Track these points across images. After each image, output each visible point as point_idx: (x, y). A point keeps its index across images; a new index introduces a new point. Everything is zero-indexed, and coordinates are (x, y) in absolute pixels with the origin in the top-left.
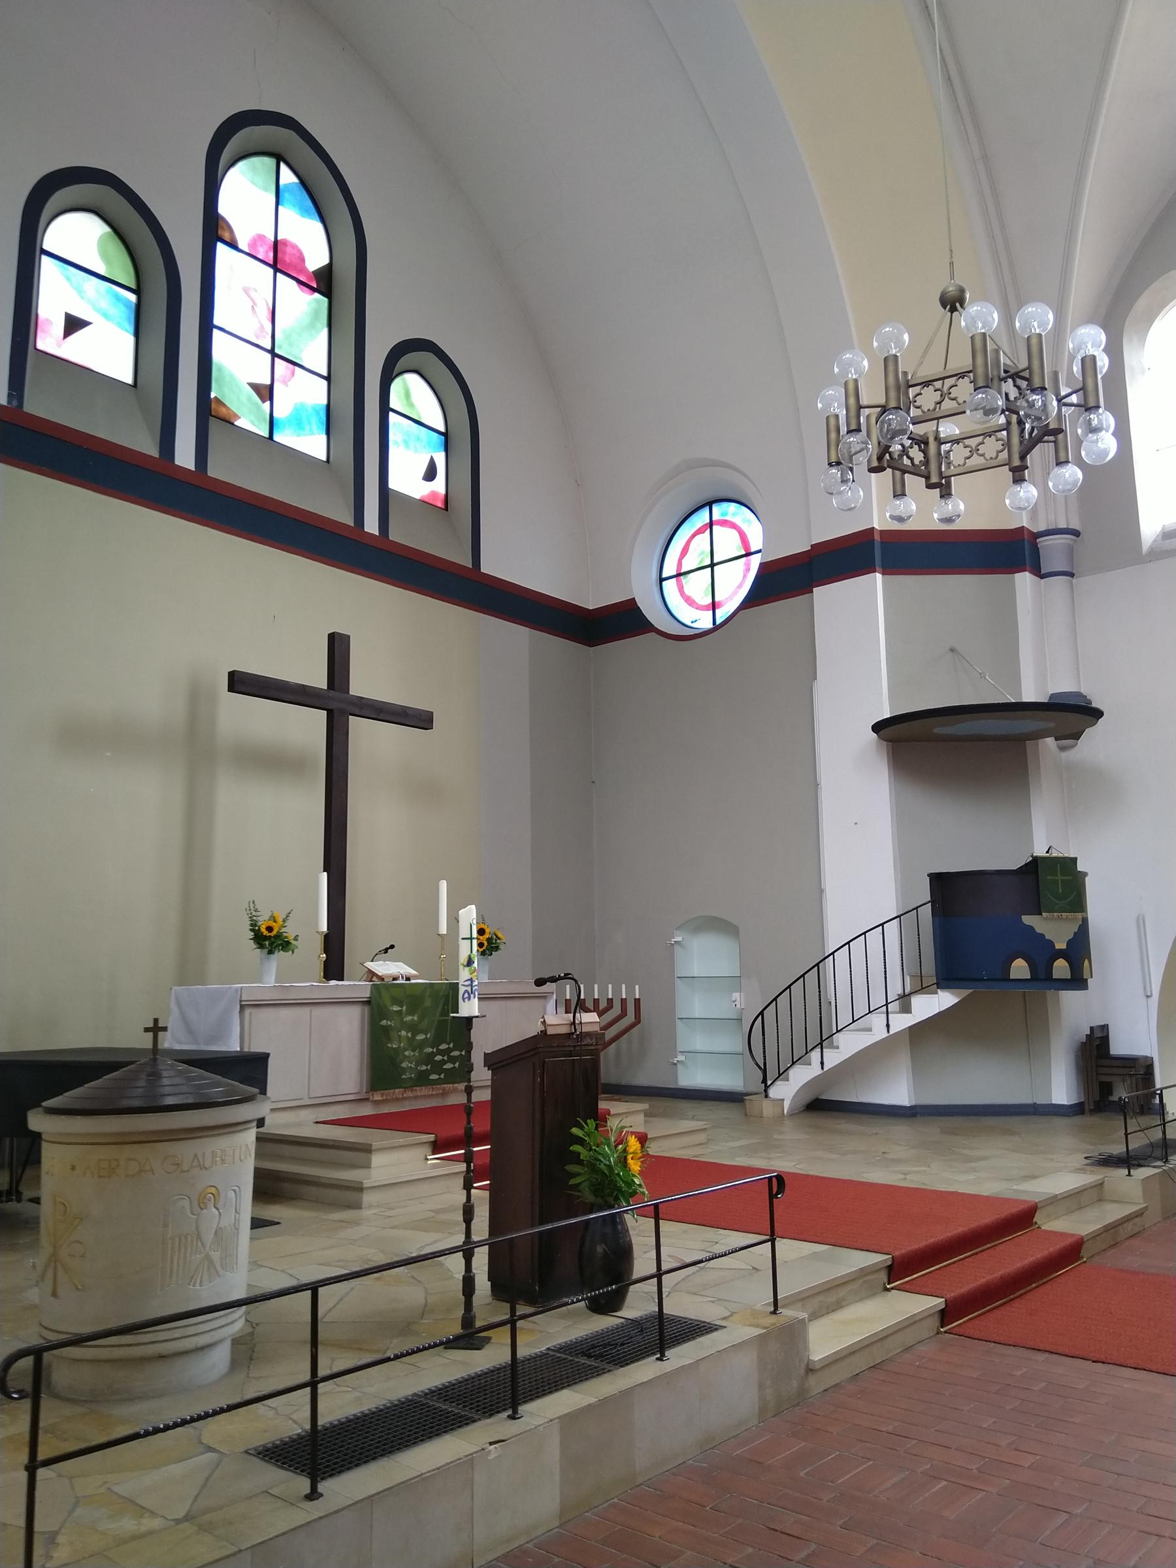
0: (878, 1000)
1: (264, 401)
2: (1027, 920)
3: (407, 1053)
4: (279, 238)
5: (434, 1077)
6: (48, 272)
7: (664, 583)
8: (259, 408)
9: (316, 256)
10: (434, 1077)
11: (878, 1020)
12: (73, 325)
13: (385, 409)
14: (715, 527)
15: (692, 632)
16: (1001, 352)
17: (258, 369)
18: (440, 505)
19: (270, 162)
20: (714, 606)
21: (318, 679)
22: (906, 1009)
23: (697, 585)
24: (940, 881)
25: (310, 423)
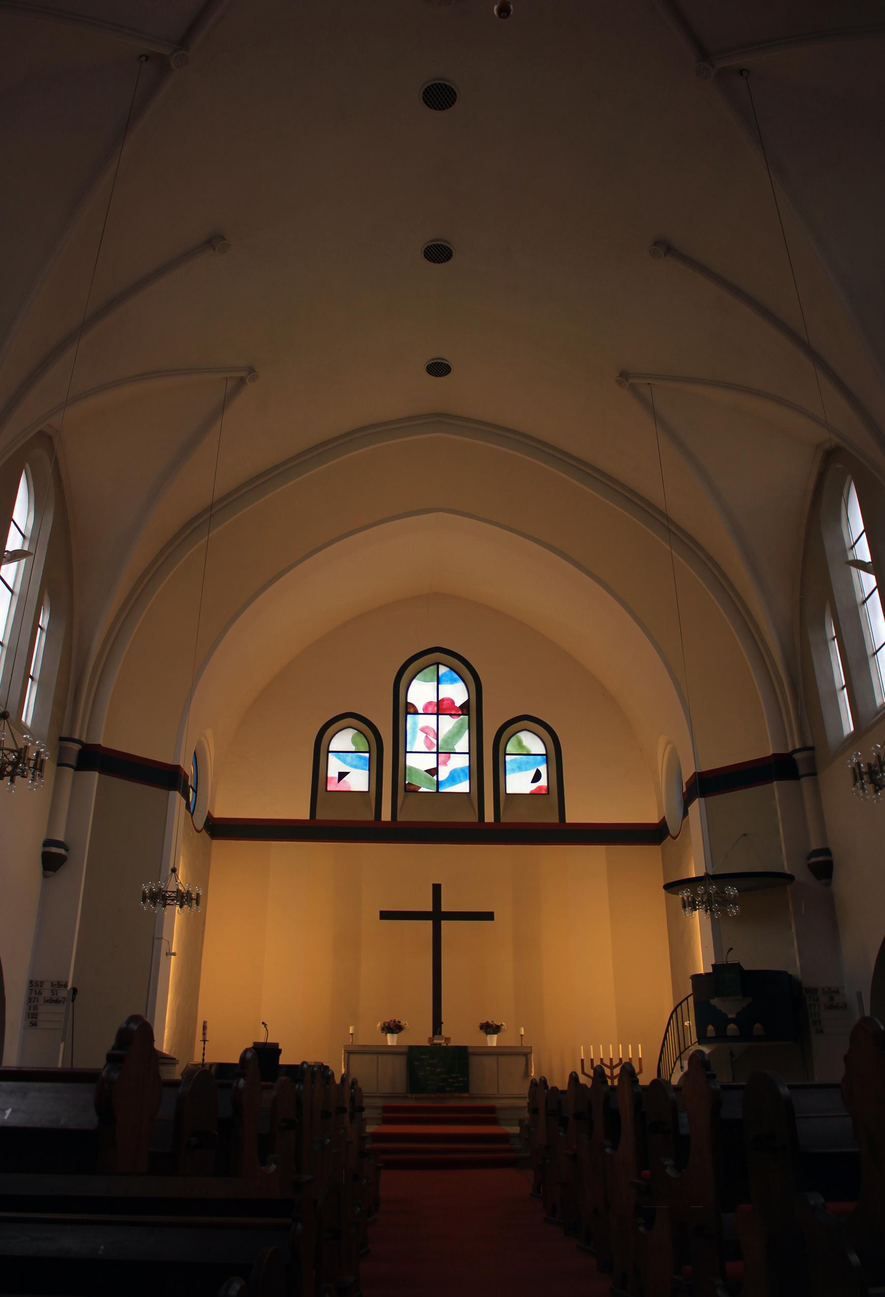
1: (433, 776)
5: (448, 1089)
8: (431, 780)
10: (448, 1089)
16: (191, 790)
17: (430, 761)
25: (459, 777)
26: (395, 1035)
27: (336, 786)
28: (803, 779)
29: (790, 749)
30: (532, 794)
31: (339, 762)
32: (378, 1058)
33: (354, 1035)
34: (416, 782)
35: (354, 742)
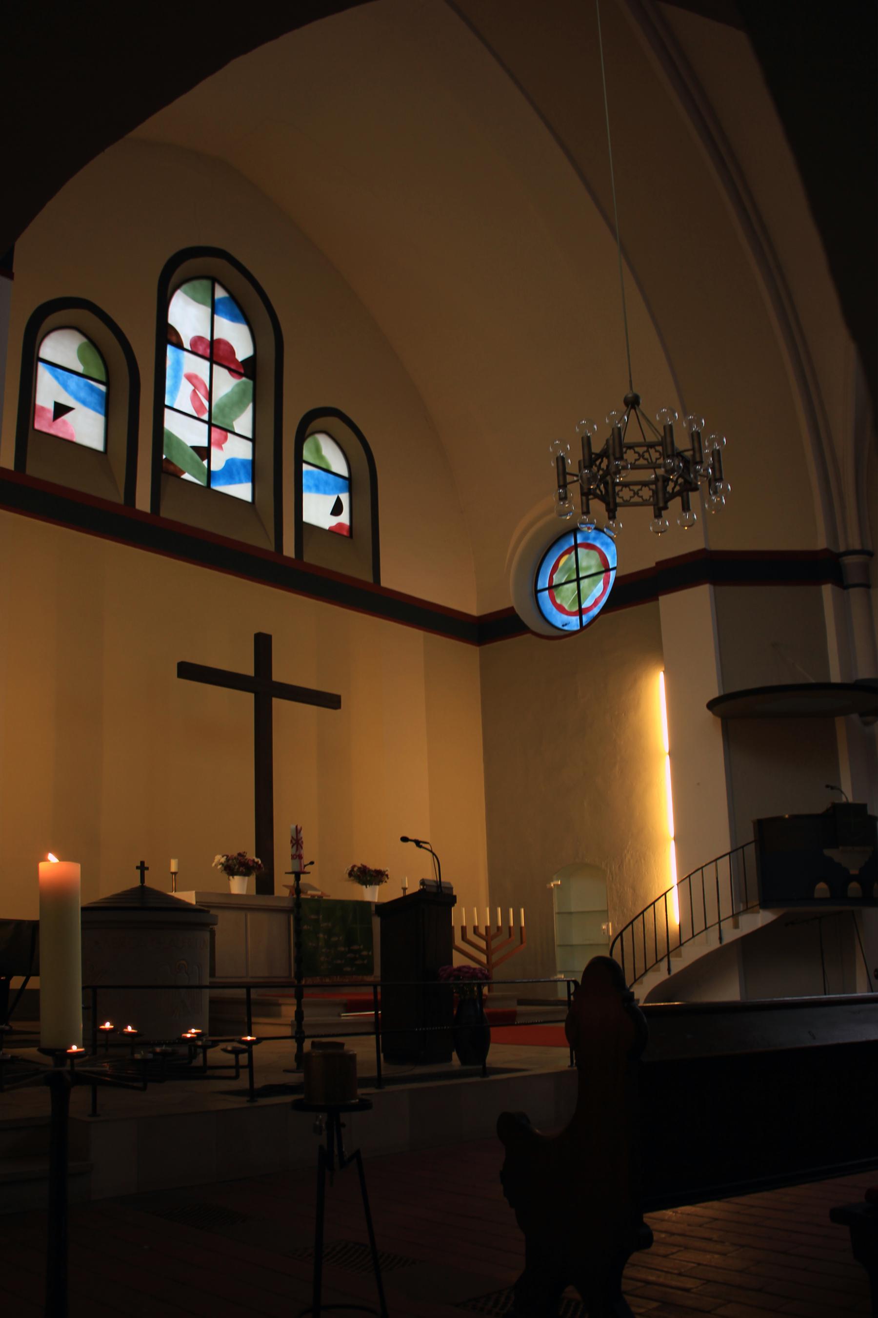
0: (712, 919)
1: (203, 460)
2: (827, 852)
3: (324, 950)
4: (215, 337)
6: (44, 375)
7: (539, 595)
9: (243, 349)
11: (714, 934)
12: (61, 410)
13: (299, 461)
14: (579, 549)
15: (562, 633)
18: (345, 533)
19: (206, 283)
20: (581, 612)
21: (247, 668)
22: (736, 926)
23: (566, 595)
24: (761, 825)
25: (239, 474)
26: (247, 878)
27: (50, 426)
28: (852, 591)
29: (842, 549)
30: (332, 531)
31: (55, 383)
32: (246, 916)
33: (177, 875)
34: (178, 462)
35: (82, 358)
